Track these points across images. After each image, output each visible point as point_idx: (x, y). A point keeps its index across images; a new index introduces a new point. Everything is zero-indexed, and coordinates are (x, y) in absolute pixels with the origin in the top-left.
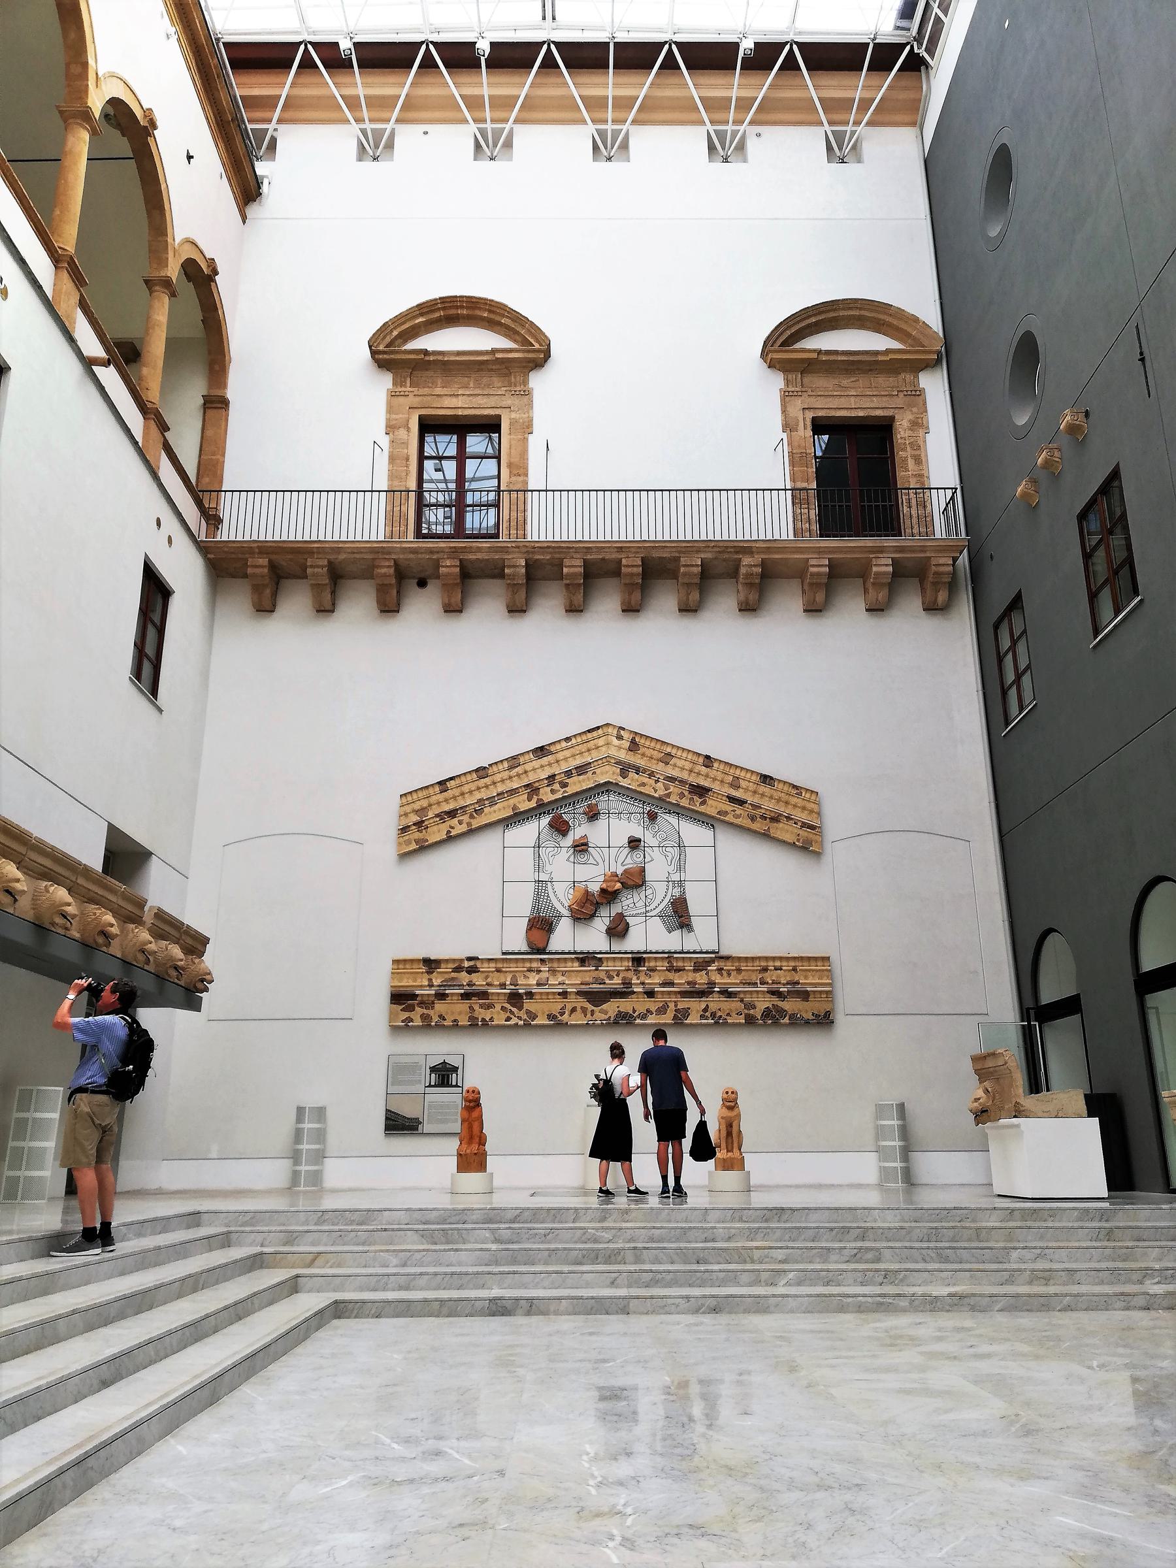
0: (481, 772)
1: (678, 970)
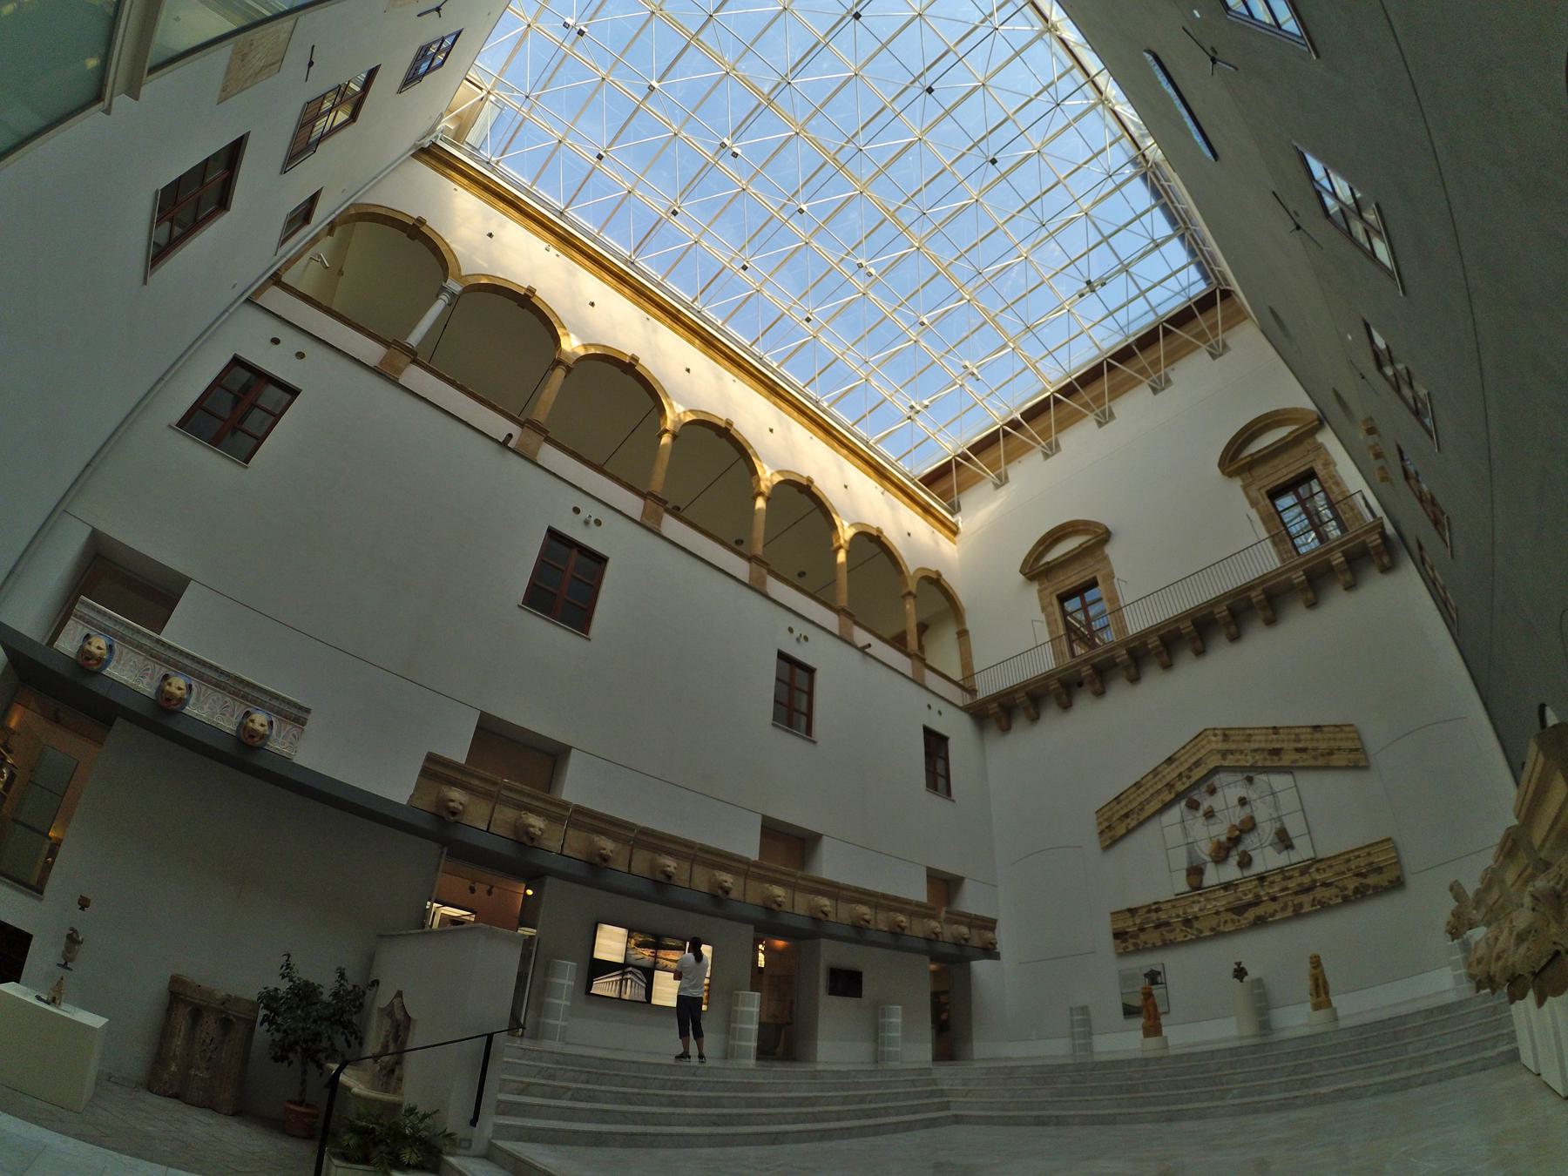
0: (1138, 785)
1: (1290, 878)
